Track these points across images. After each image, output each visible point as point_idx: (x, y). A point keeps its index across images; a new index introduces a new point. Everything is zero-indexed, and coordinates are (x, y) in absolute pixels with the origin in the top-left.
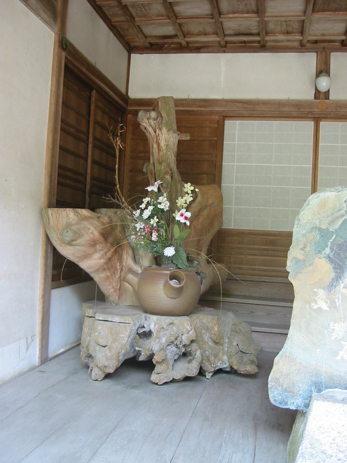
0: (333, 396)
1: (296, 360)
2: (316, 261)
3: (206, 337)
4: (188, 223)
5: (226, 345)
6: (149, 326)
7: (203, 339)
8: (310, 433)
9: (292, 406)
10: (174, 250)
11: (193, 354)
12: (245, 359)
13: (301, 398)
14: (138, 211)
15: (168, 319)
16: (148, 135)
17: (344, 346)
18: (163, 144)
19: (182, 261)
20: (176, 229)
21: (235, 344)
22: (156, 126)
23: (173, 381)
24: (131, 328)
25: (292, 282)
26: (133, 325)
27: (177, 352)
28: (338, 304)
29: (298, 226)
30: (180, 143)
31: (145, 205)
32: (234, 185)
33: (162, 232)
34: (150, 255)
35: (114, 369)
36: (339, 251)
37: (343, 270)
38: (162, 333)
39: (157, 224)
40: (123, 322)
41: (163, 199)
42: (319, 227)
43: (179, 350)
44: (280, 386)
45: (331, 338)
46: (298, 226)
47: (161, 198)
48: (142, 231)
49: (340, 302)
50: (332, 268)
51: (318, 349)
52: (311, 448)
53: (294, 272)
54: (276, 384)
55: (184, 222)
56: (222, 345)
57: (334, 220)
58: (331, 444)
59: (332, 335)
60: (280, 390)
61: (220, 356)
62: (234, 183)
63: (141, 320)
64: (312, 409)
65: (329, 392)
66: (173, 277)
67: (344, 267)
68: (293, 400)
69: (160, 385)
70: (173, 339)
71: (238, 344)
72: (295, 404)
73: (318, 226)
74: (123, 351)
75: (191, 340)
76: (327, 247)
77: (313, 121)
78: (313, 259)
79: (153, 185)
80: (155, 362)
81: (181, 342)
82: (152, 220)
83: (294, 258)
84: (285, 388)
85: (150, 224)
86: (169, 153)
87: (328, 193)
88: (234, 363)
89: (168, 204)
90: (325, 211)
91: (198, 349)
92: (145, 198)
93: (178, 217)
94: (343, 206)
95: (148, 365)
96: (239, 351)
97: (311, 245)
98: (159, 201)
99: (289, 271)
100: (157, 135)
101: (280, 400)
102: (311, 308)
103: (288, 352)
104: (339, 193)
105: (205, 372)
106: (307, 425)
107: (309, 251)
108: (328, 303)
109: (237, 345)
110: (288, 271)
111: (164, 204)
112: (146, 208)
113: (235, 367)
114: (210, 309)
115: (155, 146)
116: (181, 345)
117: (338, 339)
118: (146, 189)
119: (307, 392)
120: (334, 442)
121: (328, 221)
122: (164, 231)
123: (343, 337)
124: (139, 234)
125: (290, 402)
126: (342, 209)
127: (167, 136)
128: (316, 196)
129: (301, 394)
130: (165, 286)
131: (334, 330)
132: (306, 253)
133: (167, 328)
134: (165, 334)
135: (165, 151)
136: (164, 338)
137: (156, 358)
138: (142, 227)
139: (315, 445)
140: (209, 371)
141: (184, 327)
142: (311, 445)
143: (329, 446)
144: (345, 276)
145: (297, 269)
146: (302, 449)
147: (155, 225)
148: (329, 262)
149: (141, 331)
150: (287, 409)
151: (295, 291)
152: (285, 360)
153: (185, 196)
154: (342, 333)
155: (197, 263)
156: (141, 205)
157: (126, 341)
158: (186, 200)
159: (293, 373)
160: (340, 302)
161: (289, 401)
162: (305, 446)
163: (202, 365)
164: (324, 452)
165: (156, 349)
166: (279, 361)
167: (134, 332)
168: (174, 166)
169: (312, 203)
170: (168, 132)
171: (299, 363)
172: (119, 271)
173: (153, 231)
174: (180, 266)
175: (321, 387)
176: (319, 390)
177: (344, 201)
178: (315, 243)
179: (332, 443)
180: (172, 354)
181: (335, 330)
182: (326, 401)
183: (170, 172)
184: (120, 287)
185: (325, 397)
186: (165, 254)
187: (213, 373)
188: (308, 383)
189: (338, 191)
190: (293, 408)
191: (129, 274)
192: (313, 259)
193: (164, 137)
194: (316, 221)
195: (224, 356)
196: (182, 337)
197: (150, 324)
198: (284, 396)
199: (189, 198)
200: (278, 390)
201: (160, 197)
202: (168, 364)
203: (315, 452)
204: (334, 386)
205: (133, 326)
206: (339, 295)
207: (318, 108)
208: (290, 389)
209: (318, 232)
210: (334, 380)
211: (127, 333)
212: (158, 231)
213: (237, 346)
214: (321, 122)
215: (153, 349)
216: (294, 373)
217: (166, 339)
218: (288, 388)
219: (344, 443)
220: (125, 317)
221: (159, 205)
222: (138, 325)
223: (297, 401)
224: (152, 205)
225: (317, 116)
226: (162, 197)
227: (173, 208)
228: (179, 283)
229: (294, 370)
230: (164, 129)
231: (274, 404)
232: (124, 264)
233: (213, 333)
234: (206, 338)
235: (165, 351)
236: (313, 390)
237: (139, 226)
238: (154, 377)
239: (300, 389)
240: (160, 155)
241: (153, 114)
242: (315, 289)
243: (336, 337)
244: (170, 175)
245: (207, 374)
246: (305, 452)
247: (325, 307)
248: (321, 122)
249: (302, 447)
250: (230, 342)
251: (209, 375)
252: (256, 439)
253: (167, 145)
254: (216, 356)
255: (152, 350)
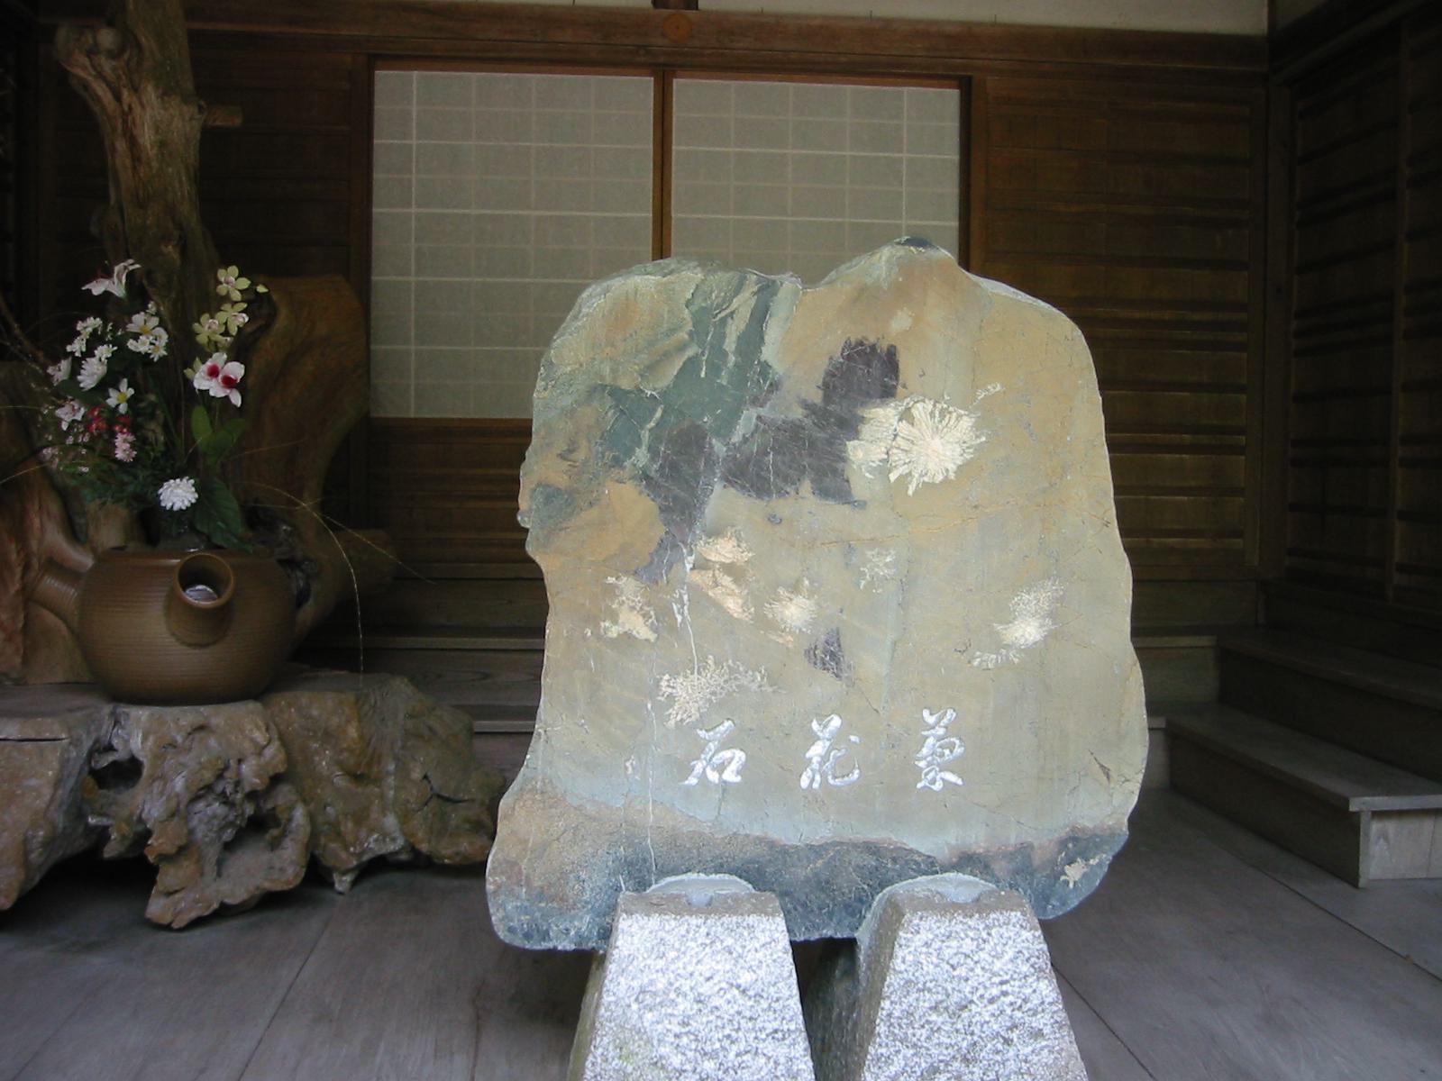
0: (679, 896)
1: (565, 799)
2: (607, 492)
3: (324, 763)
4: (236, 399)
5: (391, 780)
6: (126, 742)
7: (315, 768)
8: (615, 1014)
9: (564, 940)
10: (193, 489)
11: (283, 817)
12: (455, 818)
13: (587, 913)
14: (65, 365)
15: (182, 718)
16: (97, 109)
17: (706, 745)
18: (147, 137)
19: (227, 525)
20: (200, 421)
21: (416, 774)
22: (119, 78)
23: (224, 912)
24: (62, 754)
25: (538, 559)
26: (70, 743)
27: (231, 818)
28: (679, 618)
29: (547, 384)
30: (211, 138)
31: (84, 342)
32: (413, 279)
33: (154, 431)
34: (123, 512)
35: (14, 896)
36: (674, 458)
37: (690, 514)
38: (171, 761)
39: (129, 407)
40: (33, 736)
41: (145, 321)
42: (611, 386)
43: (236, 811)
44: (522, 883)
45: (667, 722)
46: (547, 384)
47: (139, 318)
48: (81, 430)
49: (686, 612)
50: (658, 511)
51: (628, 760)
52: (620, 1058)
53: (542, 528)
54: (509, 878)
55: (223, 395)
56: (377, 781)
57: (658, 362)
58: (677, 1036)
59: (667, 713)
60: (524, 896)
61: (374, 815)
62: (413, 268)
63: (100, 727)
64: (615, 942)
65: (668, 885)
66: (189, 577)
67: (692, 504)
68: (565, 920)
69: (181, 930)
70: (208, 776)
71: (429, 774)
72: (572, 933)
73: (608, 380)
74: (41, 833)
75: (271, 773)
76: (639, 445)
77: (650, 76)
78: (599, 484)
79: (108, 274)
80: (153, 857)
81: (238, 783)
82: (112, 392)
83: (539, 485)
84: (538, 889)
85: (108, 407)
86: (170, 170)
87: (636, 277)
88: (420, 834)
89: (165, 337)
90: (628, 335)
91: (296, 801)
92: (83, 319)
93: (201, 381)
94: (681, 316)
95: (135, 873)
96: (431, 798)
97: (589, 442)
98: (132, 328)
99: (528, 526)
100: (126, 109)
101: (525, 926)
102: (598, 637)
103: (540, 778)
104: (669, 277)
105: (330, 871)
106: (605, 989)
107: (585, 462)
108: (651, 617)
109: (426, 777)
110: (522, 525)
111: (149, 337)
112: (89, 353)
113: (424, 847)
114: (337, 672)
115: (121, 146)
116: (239, 796)
117: (688, 723)
118: (84, 288)
119: (606, 893)
120: (687, 1029)
121: (638, 365)
122: (159, 430)
123: (701, 716)
124: (70, 440)
125: (555, 928)
126: (681, 327)
127: (162, 112)
128: (599, 290)
129: (587, 903)
130: (168, 609)
131: (675, 697)
132: (576, 469)
133: (187, 743)
134: (181, 764)
135: (155, 164)
136: (180, 777)
137: (155, 844)
138: (79, 417)
139: (631, 1048)
140: (343, 868)
141: (245, 736)
142: (621, 1049)
143: (672, 1044)
144: (698, 532)
145: (551, 521)
146: (593, 1064)
147: (123, 409)
148: (647, 491)
149: (105, 761)
150: (549, 950)
151: (548, 588)
152: (533, 803)
153: (222, 308)
154: (696, 705)
155: (289, 529)
156: (71, 343)
157: (48, 797)
158: (226, 324)
159: (558, 839)
160: (686, 612)
161: (552, 925)
162: (602, 1054)
163: (317, 852)
164: (659, 1065)
165: (156, 815)
166: (514, 809)
167: (78, 767)
168: (188, 212)
169: (587, 310)
170: (162, 99)
171: (575, 808)
172: (18, 571)
173: (117, 428)
174: (218, 540)
175: (646, 874)
176: (639, 882)
177: (683, 301)
178: (603, 435)
179: (681, 1033)
180: (213, 825)
181: (676, 699)
182: (656, 912)
183: (176, 233)
184: (25, 625)
185: (654, 901)
186: (163, 504)
187: (357, 872)
188: (607, 867)
189: (666, 271)
190: (566, 945)
191: (46, 577)
192: (599, 484)
193: (152, 117)
194: (602, 366)
195: (385, 815)
196: (239, 769)
197: (129, 734)
198: (538, 914)
199: (237, 318)
200: (518, 898)
201: (135, 313)
202: (200, 860)
203: (634, 1069)
204: (683, 867)
205: (71, 748)
206: (682, 591)
207: (664, 35)
208: (553, 890)
209: (609, 402)
210: (682, 848)
211: (50, 773)
212: (134, 428)
213: (425, 781)
214: (675, 80)
215: (144, 816)
216: (562, 840)
217: (186, 781)
218: (546, 888)
219: (714, 1029)
220: (40, 719)
221: (131, 341)
222: (91, 743)
223: (576, 923)
224: (108, 343)
225: (662, 60)
226: (142, 313)
227: (186, 349)
228: (216, 596)
229: (562, 829)
230: (150, 88)
231: (507, 941)
232: (34, 545)
233: (345, 745)
234: (323, 763)
235: (187, 819)
236: (623, 886)
237: (69, 414)
238: (157, 908)
239: (583, 888)
240: (139, 177)
241: (107, 38)
242: (609, 578)
243: (679, 718)
244: (175, 242)
245: (336, 877)
246: (603, 1072)
247: (643, 631)
248: (675, 80)
249: (595, 1057)
250: (403, 771)
251: (342, 882)
252: (476, 1057)
253: (161, 142)
254: (360, 818)
255: (140, 820)
